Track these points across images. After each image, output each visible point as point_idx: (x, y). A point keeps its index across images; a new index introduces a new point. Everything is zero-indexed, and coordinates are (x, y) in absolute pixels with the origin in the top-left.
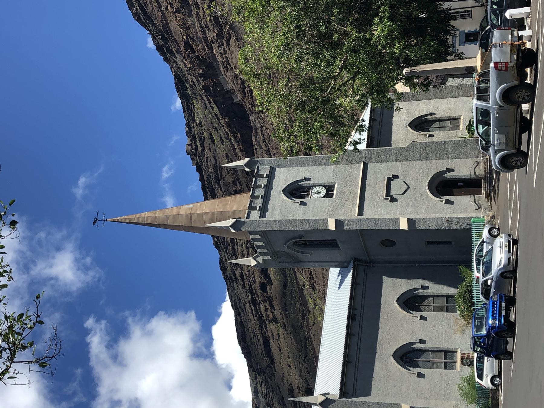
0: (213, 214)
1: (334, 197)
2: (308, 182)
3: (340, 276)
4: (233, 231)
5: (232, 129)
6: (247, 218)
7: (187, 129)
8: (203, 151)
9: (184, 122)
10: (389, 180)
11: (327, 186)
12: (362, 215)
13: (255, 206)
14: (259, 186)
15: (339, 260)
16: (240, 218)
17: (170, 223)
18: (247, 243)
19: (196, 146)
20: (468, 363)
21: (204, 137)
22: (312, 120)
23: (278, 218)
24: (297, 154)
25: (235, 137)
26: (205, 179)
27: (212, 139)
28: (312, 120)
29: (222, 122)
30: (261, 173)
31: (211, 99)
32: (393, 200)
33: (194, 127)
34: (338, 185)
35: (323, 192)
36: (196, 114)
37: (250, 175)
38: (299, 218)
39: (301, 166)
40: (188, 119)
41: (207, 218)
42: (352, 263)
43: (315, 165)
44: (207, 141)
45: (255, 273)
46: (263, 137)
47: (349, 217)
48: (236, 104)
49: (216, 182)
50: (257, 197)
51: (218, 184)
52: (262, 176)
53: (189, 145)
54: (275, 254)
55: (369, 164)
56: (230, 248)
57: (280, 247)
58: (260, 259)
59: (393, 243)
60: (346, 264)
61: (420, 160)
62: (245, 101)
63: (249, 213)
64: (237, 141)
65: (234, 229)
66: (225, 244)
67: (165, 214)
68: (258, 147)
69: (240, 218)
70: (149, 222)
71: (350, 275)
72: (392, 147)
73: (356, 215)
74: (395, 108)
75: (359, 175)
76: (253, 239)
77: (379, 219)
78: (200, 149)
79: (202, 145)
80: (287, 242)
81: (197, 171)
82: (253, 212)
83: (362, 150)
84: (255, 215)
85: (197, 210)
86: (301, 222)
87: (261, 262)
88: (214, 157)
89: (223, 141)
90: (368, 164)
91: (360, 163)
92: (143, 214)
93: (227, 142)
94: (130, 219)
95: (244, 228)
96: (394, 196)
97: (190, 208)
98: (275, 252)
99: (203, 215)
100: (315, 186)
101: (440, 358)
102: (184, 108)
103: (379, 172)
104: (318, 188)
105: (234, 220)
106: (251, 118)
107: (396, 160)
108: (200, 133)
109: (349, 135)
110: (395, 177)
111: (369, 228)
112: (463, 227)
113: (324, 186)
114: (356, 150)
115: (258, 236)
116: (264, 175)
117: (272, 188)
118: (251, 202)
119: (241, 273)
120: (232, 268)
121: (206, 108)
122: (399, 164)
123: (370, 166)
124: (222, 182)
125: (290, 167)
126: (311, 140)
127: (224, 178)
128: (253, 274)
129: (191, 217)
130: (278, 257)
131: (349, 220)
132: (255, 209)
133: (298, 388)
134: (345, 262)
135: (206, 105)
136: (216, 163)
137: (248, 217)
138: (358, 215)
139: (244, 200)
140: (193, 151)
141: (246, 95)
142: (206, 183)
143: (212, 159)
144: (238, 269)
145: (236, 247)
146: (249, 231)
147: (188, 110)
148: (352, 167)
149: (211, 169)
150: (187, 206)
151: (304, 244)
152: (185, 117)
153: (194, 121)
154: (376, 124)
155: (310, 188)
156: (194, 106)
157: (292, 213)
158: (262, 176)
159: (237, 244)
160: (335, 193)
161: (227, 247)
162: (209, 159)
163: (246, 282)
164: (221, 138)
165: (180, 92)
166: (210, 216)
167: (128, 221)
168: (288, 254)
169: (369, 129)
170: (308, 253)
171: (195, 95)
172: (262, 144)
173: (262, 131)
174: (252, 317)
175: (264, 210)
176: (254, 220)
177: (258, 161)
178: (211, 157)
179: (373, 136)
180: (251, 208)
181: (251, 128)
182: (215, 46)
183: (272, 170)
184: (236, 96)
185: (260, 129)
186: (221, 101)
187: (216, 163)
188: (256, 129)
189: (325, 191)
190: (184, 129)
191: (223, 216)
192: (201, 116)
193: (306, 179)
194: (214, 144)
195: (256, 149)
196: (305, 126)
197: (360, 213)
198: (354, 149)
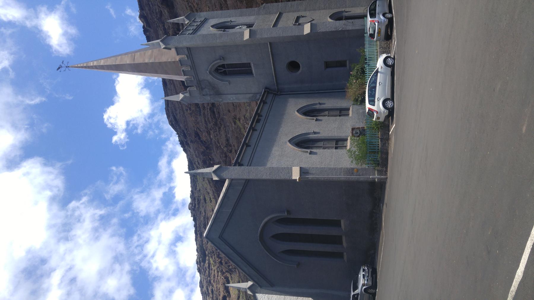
8: (199, 207)
10: (298, 18)
19: (195, 204)
20: (357, 133)
26: (198, 226)
27: (205, 200)
56: (207, 272)
61: (324, 9)
78: (197, 206)
79: (199, 204)
88: (205, 211)
90: (283, 13)
91: (276, 13)
100: (237, 26)
101: (334, 144)
112: (357, 28)
134: (257, 93)
149: (202, 218)
163: (214, 296)
182: (212, 132)
194: (206, 203)
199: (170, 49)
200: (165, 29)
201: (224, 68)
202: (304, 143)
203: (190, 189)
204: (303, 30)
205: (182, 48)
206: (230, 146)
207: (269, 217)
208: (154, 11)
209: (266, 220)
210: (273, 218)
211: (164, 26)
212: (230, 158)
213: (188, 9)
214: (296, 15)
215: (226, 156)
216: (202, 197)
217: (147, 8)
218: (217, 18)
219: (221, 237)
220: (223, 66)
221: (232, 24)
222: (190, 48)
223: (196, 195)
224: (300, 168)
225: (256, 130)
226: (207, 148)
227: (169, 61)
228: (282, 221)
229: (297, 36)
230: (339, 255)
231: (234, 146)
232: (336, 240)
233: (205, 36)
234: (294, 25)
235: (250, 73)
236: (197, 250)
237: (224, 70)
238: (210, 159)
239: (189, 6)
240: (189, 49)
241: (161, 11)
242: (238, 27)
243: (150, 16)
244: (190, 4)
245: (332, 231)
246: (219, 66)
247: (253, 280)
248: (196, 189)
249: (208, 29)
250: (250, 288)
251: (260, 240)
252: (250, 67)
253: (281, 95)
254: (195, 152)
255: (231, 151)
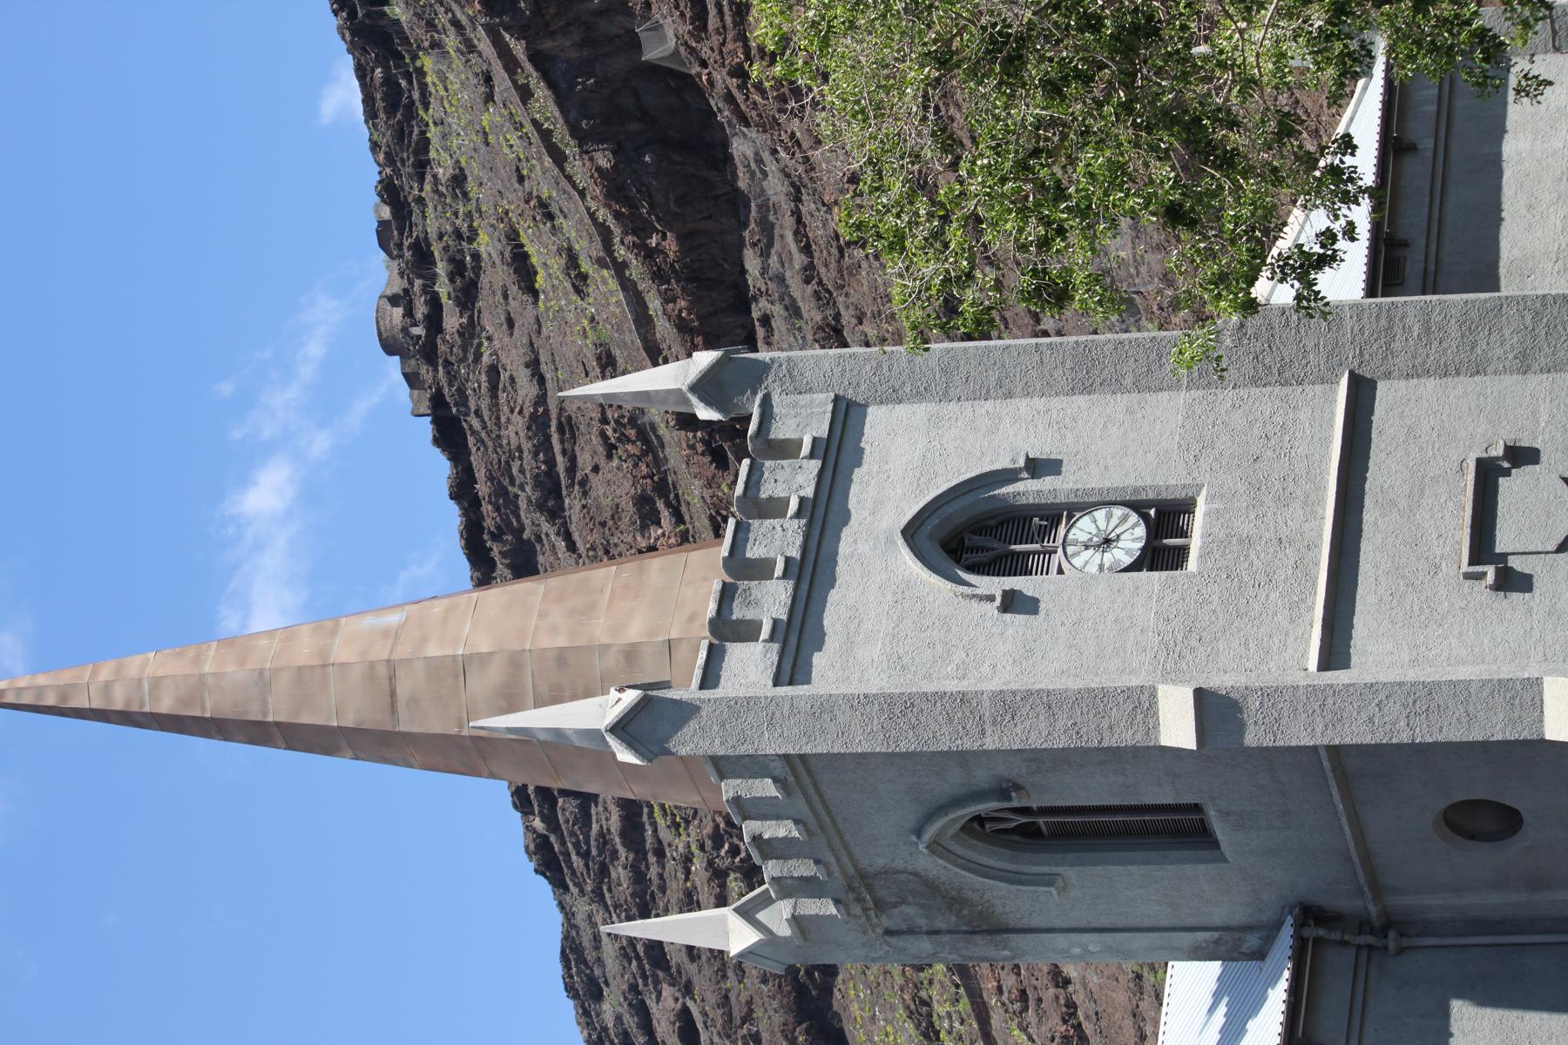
0: (515, 662)
1: (1193, 563)
2: (1047, 483)
3: (1222, 1009)
4: (625, 756)
5: (633, 206)
6: (702, 687)
7: (386, 212)
8: (470, 331)
9: (369, 172)
10: (1488, 475)
11: (1149, 504)
12: (1345, 664)
13: (750, 615)
14: (774, 508)
15: (1219, 916)
16: (665, 685)
17: (278, 711)
18: (718, 845)
19: (435, 304)
21: (476, 257)
22: (1064, 137)
23: (877, 682)
24: (982, 329)
25: (649, 254)
26: (483, 488)
27: (521, 264)
28: (1064, 137)
29: (579, 169)
30: (782, 430)
31: (518, 48)
32: (1511, 581)
33: (420, 201)
34: (1210, 498)
35: (1133, 537)
36: (433, 133)
37: (724, 444)
38: (995, 685)
39: (1009, 395)
40: (390, 160)
41: (482, 683)
42: (1287, 931)
43: (1087, 390)
44: (496, 276)
45: (758, 1013)
46: (807, 250)
47: (1271, 674)
48: (655, 71)
49: (540, 507)
50: (762, 570)
51: (556, 514)
52: (786, 449)
53: (394, 300)
54: (864, 891)
55: (1382, 388)
56: (620, 873)
57: (892, 843)
58: (778, 917)
59: (1507, 821)
60: (1252, 941)
62: (705, 53)
63: (715, 657)
64: (658, 276)
65: (632, 744)
66: (588, 837)
67: (250, 665)
68: (778, 310)
69: (665, 685)
70: (165, 705)
71: (1277, 996)
72: (1504, 293)
73: (1313, 662)
74: (1513, 81)
75: (1327, 441)
76: (736, 801)
77: (1431, 688)
78: (452, 321)
80: (930, 817)
81: (437, 441)
82: (737, 653)
83: (1340, 306)
84: (749, 666)
85: (424, 640)
86: (1008, 705)
87: (784, 930)
88: (534, 365)
89: (584, 277)
91: (1329, 380)
92: (133, 665)
94: (64, 692)
95: (689, 742)
96: (1515, 563)
97: (385, 633)
98: (863, 876)
99: (463, 667)
100: (1087, 507)
102: (368, 101)
103: (1434, 427)
104: (1100, 514)
105: (631, 696)
106: (741, 148)
107: (1524, 365)
108: (458, 235)
109: (1269, 224)
110: (1521, 456)
111: (1380, 737)
113: (1138, 507)
114: (1308, 300)
115: (766, 788)
116: (800, 443)
117: (845, 518)
118: (727, 595)
119: (684, 1014)
120: (634, 988)
121: (489, 98)
122: (1537, 383)
123: (1385, 394)
124: (573, 504)
125: (946, 397)
126: (1059, 244)
127: (584, 483)
128: (748, 1017)
129: (392, 678)
130: (881, 906)
131: (1269, 694)
132: (747, 632)
135: (488, 79)
136: (541, 399)
137: (709, 678)
138: (1326, 664)
139: (685, 583)
140: (418, 331)
141: (713, 22)
142: (486, 508)
143: (523, 376)
144: (667, 991)
145: (653, 872)
146: (715, 760)
147: (392, 108)
148: (1285, 400)
149: (515, 431)
150: (369, 621)
151: (1023, 830)
152: (375, 146)
153: (422, 166)
154: (1416, 171)
155: (1054, 516)
156: (423, 87)
157: (959, 656)
158: (786, 449)
159: (660, 853)
160: (1195, 543)
161: (604, 871)
162: (504, 376)
164: (572, 260)
165: (352, 14)
166: (495, 674)
167: (51, 700)
168: (931, 888)
169: (1375, 193)
170: (1048, 881)
171: (431, 25)
172: (801, 293)
173: (799, 220)
175: (797, 643)
176: (742, 693)
177: (765, 368)
178: (514, 364)
179: (1402, 234)
180: (727, 629)
181: (736, 203)
183: (847, 415)
184: (657, 27)
185: (787, 207)
186: (573, 54)
187: (541, 399)
188: (765, 207)
189: (1141, 531)
190: (369, 210)
191: (568, 677)
192: (464, 141)
193: (1036, 467)
194: (535, 294)
195: (766, 320)
196: (1022, 167)
197: (1335, 652)
198: (1299, 298)
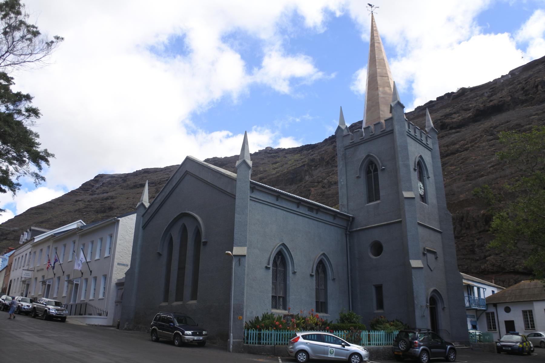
10: (434, 253)
27: (276, 163)
64: (278, 176)
78: (269, 155)
79: (272, 157)
93: (274, 172)
110: (436, 258)
129: (385, 77)
133: (113, 203)
174: (160, 178)
194: (273, 164)
199: (391, 112)
200: (451, 114)
201: (374, 171)
202: (281, 261)
203: (286, 148)
204: (416, 258)
205: (392, 125)
206: (329, 187)
207: (201, 222)
208: (470, 102)
209: (199, 219)
210: (200, 226)
211: (455, 113)
212: (317, 186)
213: (473, 137)
214: (439, 250)
215: (318, 182)
216: (278, 159)
217: (472, 95)
218: (433, 162)
219: (187, 173)
220: (376, 170)
221: (426, 178)
222: (393, 133)
223: (281, 154)
224: (245, 256)
225: (298, 207)
226: (328, 163)
227: (381, 112)
228: (198, 233)
229: (408, 252)
230: (166, 299)
231: (329, 190)
232: (179, 297)
233: (406, 148)
234: (424, 249)
235: (370, 200)
236: (226, 158)
237: (372, 171)
238: (316, 166)
239: (476, 138)
240: (392, 132)
241: (470, 110)
242: (422, 185)
243: (464, 98)
244: (478, 139)
245: (187, 291)
246: (376, 166)
247: (150, 207)
248: (287, 153)
249: (415, 151)
250: (142, 205)
251: (182, 213)
252: (376, 200)
253: (346, 234)
254: (323, 151)
255: (323, 187)
